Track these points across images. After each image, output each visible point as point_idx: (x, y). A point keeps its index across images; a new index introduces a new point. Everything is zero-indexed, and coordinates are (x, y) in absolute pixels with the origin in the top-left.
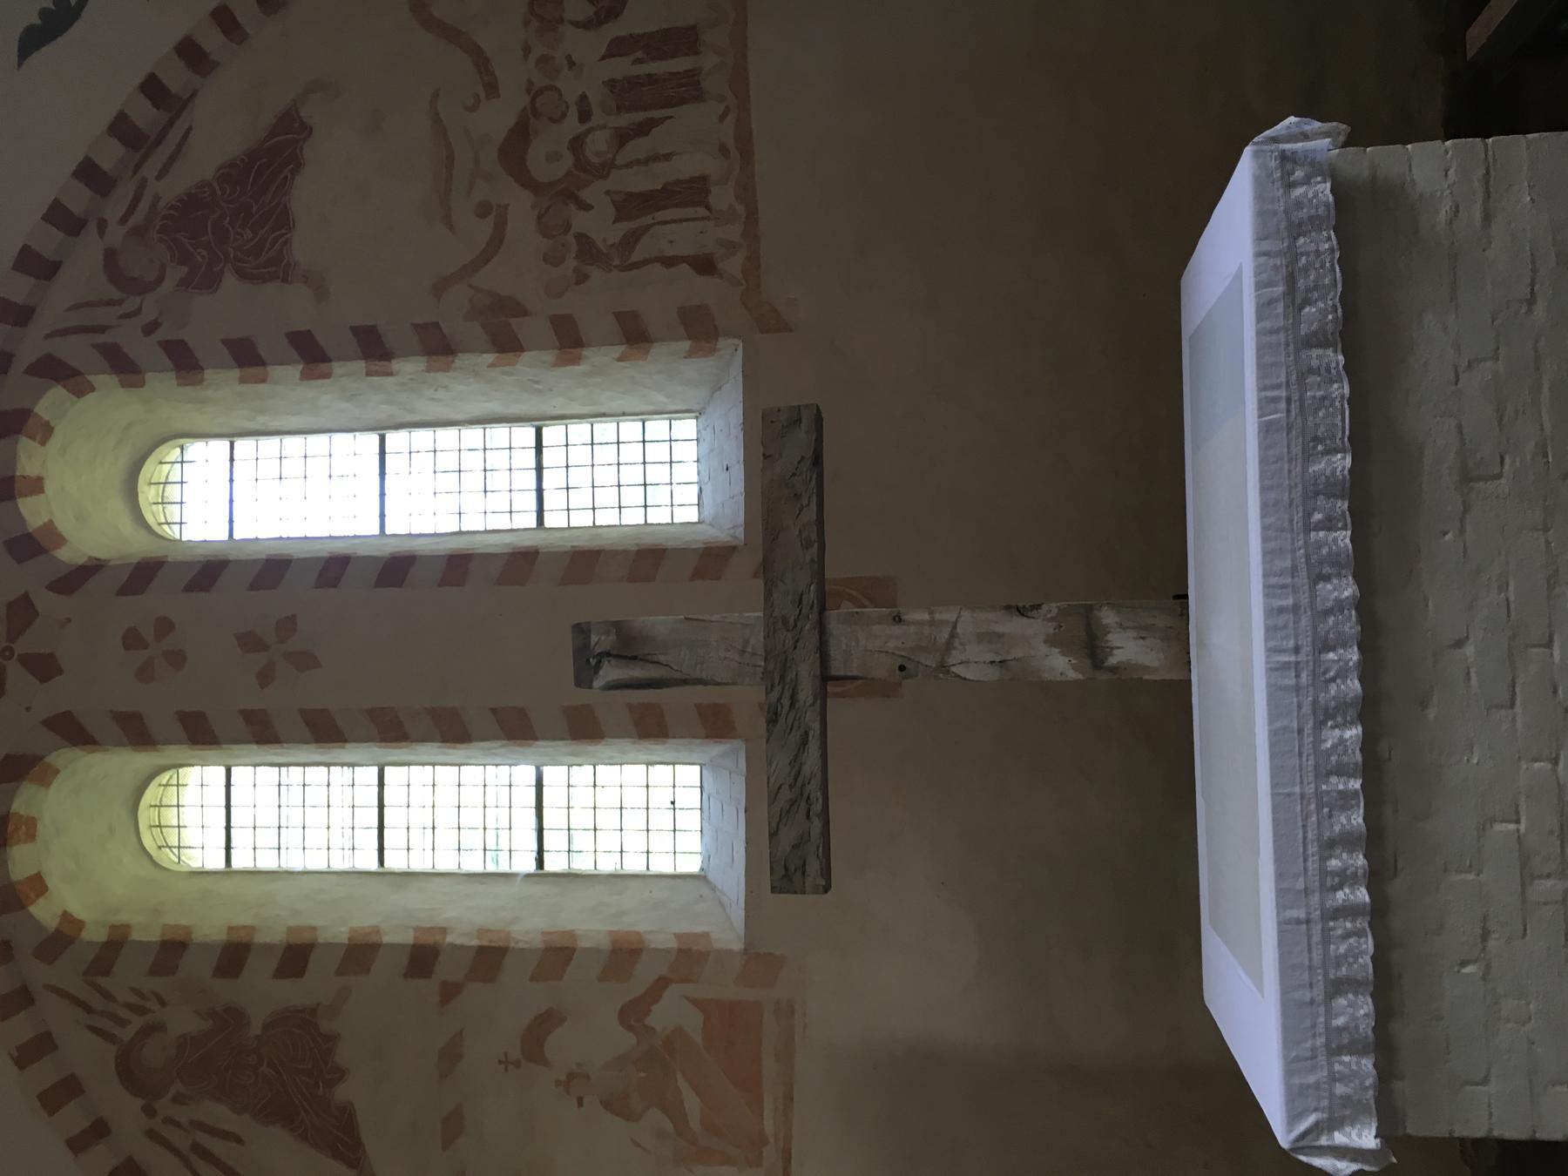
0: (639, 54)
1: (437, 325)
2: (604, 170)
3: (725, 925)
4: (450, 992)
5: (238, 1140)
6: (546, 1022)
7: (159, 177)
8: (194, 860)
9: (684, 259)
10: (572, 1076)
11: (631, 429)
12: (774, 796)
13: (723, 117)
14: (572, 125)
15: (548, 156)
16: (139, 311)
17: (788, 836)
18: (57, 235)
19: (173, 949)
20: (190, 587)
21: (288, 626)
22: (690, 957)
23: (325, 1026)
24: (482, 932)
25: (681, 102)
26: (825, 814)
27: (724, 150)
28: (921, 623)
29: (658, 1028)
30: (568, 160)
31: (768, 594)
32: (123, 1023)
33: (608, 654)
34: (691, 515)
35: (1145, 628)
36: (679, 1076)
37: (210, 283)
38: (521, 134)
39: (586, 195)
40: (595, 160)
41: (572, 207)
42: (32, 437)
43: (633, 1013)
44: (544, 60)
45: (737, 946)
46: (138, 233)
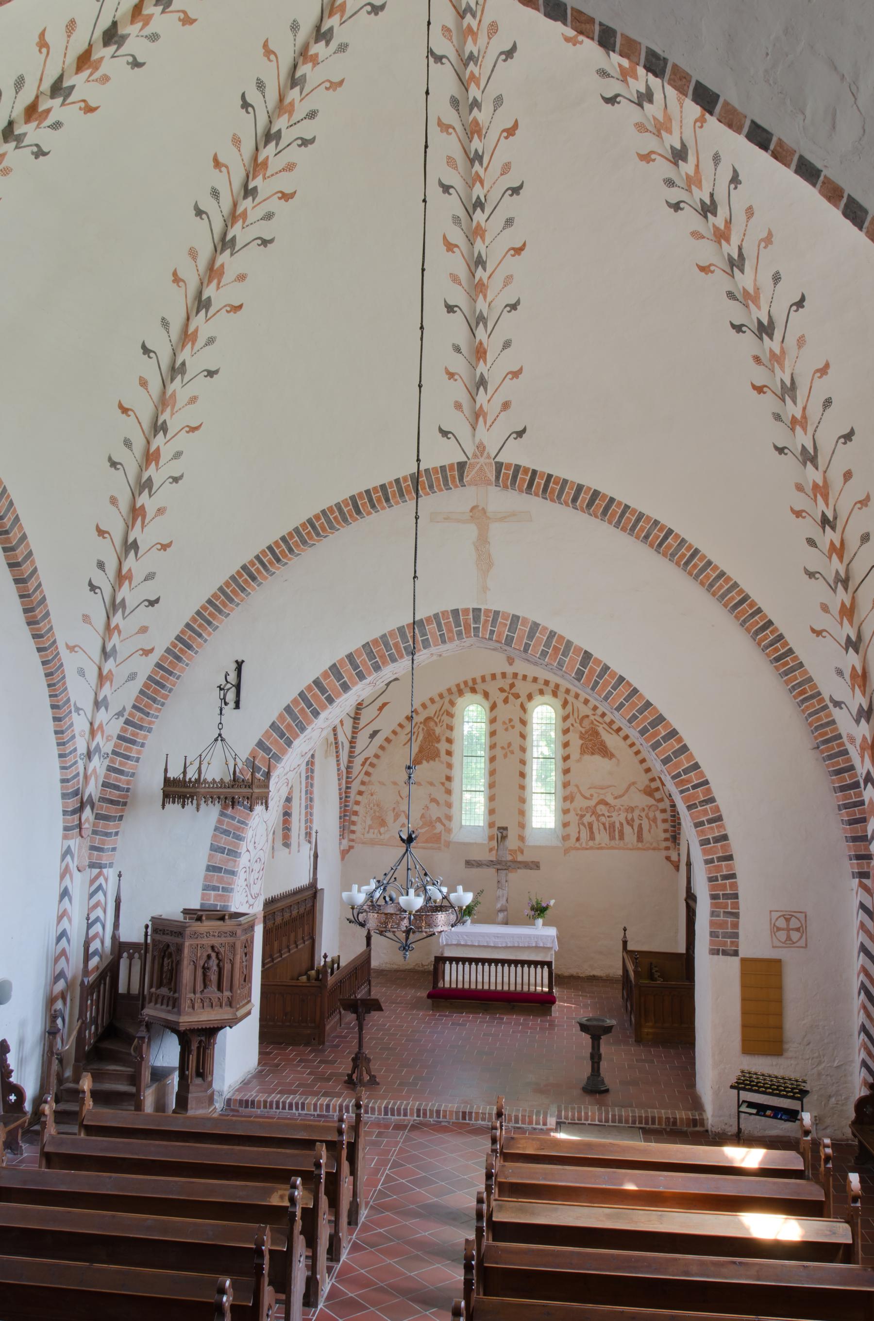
2: (598, 820)
4: (443, 784)
6: (438, 803)
14: (607, 814)
15: (601, 809)
19: (451, 728)
21: (512, 752)
22: (449, 831)
37: (581, 738)
38: (606, 804)
43: (439, 820)
44: (620, 809)
46: (592, 723)
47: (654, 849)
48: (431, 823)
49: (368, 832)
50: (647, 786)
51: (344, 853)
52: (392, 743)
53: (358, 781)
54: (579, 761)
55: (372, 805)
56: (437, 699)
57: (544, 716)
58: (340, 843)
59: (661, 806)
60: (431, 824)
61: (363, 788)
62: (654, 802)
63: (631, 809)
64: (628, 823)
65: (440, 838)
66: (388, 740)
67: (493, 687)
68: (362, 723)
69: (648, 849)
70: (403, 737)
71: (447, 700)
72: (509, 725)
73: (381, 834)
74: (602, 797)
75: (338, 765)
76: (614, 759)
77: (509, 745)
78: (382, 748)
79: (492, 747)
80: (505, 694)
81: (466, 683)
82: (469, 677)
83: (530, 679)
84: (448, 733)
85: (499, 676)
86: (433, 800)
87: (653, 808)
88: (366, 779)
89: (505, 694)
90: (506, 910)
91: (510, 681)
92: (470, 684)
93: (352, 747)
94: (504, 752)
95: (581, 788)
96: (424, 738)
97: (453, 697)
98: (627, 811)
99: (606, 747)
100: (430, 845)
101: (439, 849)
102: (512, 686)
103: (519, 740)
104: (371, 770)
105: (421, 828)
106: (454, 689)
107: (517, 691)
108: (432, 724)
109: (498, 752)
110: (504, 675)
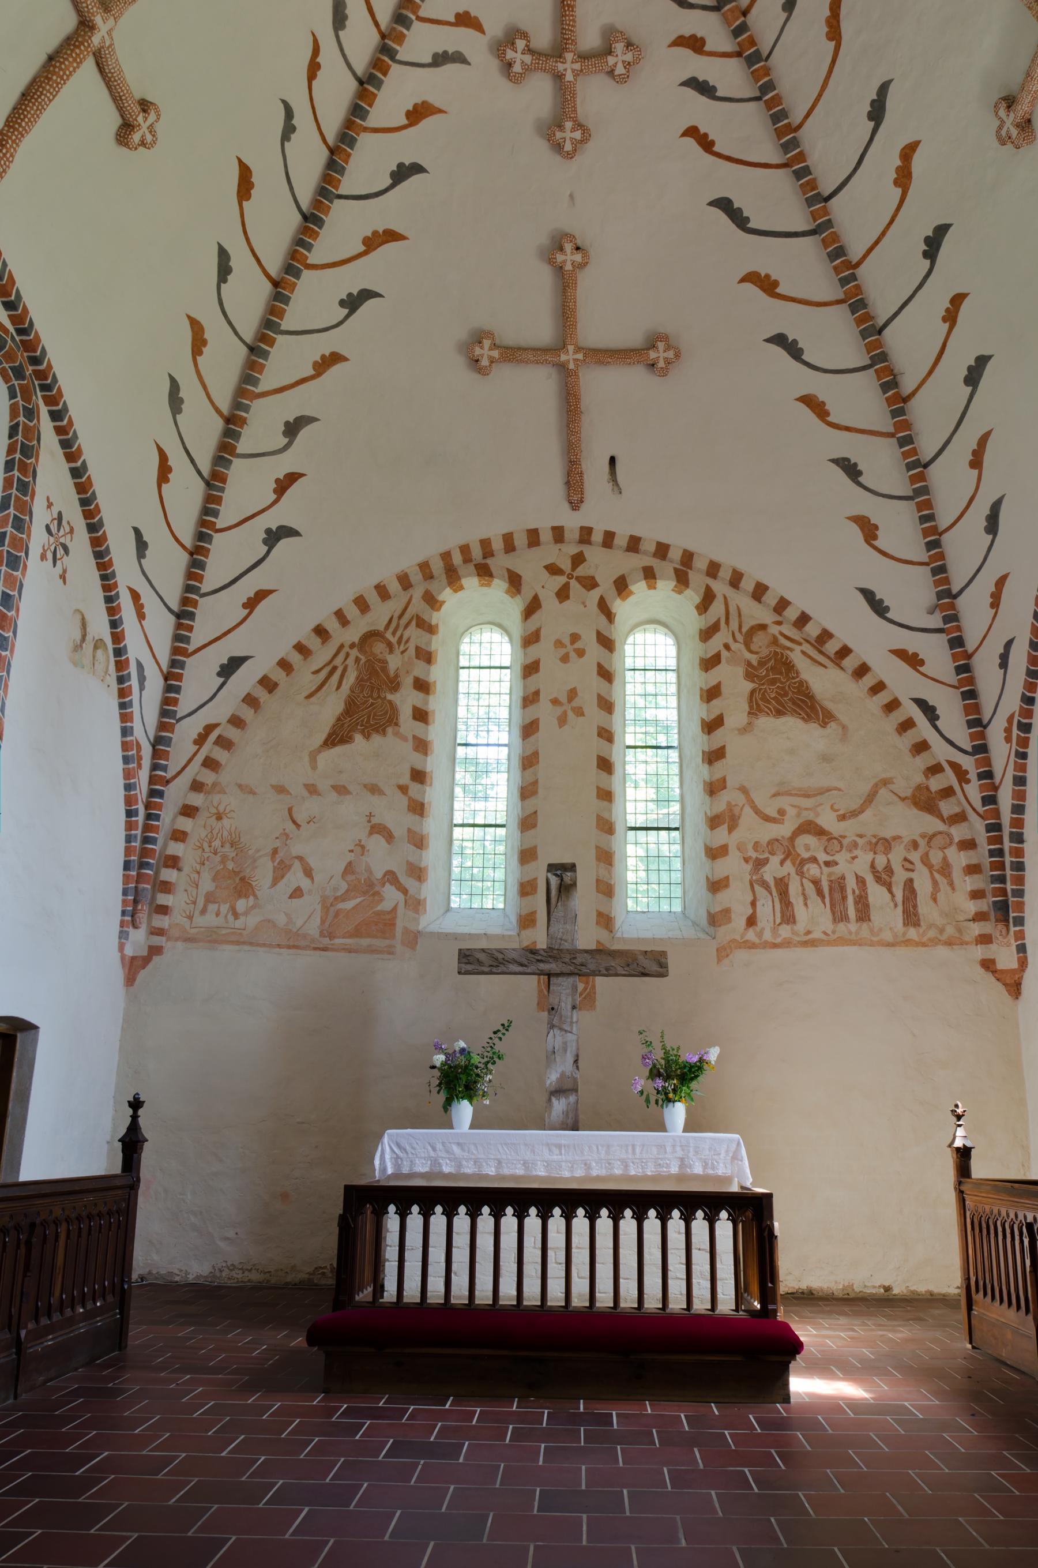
0: (857, 892)
1: (725, 788)
2: (800, 873)
3: (430, 921)
4: (403, 789)
5: (338, 688)
6: (389, 837)
7: (803, 653)
8: (464, 648)
9: (755, 912)
10: (363, 847)
11: (677, 877)
12: (499, 951)
13: (825, 933)
14: (822, 857)
16: (735, 640)
17: (482, 957)
18: (773, 602)
19: (427, 657)
20: (600, 666)
21: (579, 712)
22: (417, 905)
23: (390, 730)
24: (430, 803)
25: (833, 913)
26: (491, 973)
27: (809, 932)
28: (572, 1018)
29: (384, 889)
30: (806, 855)
31: (586, 951)
32: (394, 634)
33: (562, 880)
34: (631, 905)
35: (567, 1115)
36: (362, 898)
37: (749, 676)
38: (821, 832)
39: (788, 863)
40: (805, 869)
41: (782, 857)
42: (676, 586)
43: (391, 877)
44: (855, 845)
45: (420, 928)
46: (775, 641)
47: (949, 943)
48: (370, 884)
49: (203, 912)
50: (919, 788)
51: (134, 967)
52: (279, 691)
53: (182, 783)
54: (744, 730)
55: (217, 843)
56: (394, 587)
57: (653, 661)
58: (123, 935)
59: (958, 832)
60: (370, 889)
61: (196, 799)
62: (941, 827)
63: (885, 844)
64: (878, 879)
65: (392, 924)
66: (267, 684)
67: (530, 564)
68: (201, 632)
69: (934, 942)
70: (305, 677)
71: (417, 593)
72: (571, 648)
73: (236, 915)
74: (810, 816)
75: (126, 718)
76: (833, 725)
77: (572, 694)
78: (250, 700)
79: (529, 699)
80: (562, 580)
81: (465, 550)
82: (472, 538)
83: (621, 541)
84: (419, 669)
85: (546, 536)
86: (379, 829)
87: (939, 840)
88: (208, 777)
89: (562, 580)
90: (575, 1090)
91: (574, 550)
92: (477, 553)
93: (169, 688)
94: (559, 710)
95: (754, 795)
96: (359, 680)
97: (433, 586)
98: (873, 847)
99: (812, 698)
100: (365, 942)
101: (390, 951)
102: (578, 559)
103: (597, 683)
104: (220, 755)
105: (344, 898)
106: (437, 567)
107: (590, 572)
108: (379, 648)
109: (545, 712)
110: (558, 534)
